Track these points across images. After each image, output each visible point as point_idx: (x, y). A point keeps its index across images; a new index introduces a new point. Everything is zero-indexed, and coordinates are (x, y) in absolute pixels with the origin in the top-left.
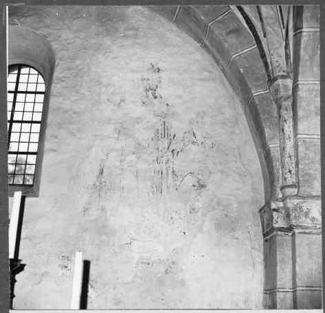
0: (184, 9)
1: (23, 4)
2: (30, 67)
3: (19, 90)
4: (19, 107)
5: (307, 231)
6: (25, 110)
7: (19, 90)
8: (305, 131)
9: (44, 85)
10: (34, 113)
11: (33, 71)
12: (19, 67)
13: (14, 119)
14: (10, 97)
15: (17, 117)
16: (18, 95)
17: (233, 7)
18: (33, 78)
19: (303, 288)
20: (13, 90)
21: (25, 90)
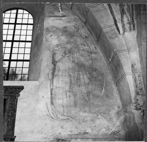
1: (49, 3)
2: (24, 9)
3: (17, 23)
6: (24, 67)
7: (17, 23)
9: (33, 19)
11: (25, 12)
13: (14, 25)
14: (4, 49)
16: (12, 62)
17: (106, 5)
18: (26, 16)
19: (128, 74)
20: (8, 58)
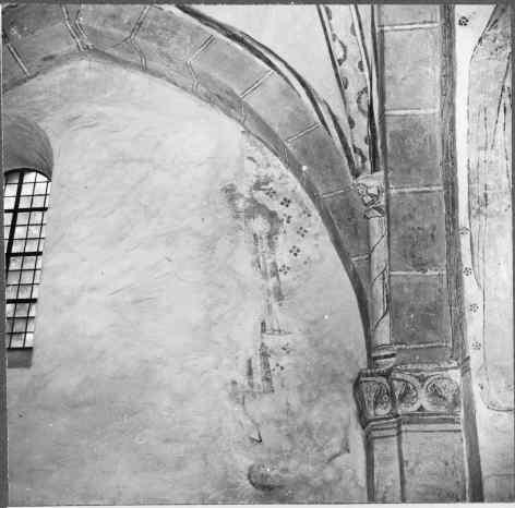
0: (376, 404)
4: (20, 232)
5: (434, 345)
8: (195, 34)
10: (25, 237)
12: (22, 173)
15: (15, 249)
20: (12, 207)
21: (33, 213)
